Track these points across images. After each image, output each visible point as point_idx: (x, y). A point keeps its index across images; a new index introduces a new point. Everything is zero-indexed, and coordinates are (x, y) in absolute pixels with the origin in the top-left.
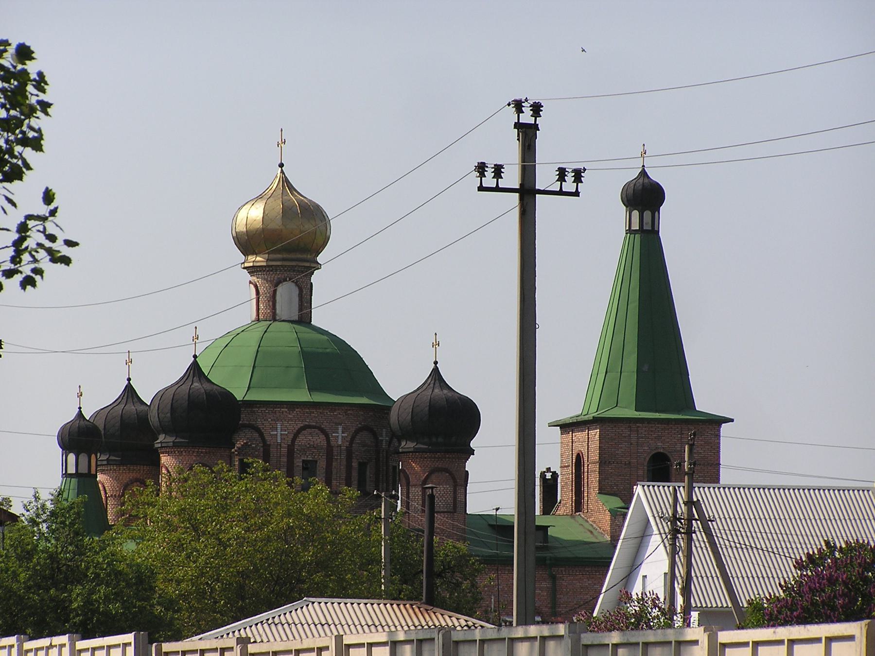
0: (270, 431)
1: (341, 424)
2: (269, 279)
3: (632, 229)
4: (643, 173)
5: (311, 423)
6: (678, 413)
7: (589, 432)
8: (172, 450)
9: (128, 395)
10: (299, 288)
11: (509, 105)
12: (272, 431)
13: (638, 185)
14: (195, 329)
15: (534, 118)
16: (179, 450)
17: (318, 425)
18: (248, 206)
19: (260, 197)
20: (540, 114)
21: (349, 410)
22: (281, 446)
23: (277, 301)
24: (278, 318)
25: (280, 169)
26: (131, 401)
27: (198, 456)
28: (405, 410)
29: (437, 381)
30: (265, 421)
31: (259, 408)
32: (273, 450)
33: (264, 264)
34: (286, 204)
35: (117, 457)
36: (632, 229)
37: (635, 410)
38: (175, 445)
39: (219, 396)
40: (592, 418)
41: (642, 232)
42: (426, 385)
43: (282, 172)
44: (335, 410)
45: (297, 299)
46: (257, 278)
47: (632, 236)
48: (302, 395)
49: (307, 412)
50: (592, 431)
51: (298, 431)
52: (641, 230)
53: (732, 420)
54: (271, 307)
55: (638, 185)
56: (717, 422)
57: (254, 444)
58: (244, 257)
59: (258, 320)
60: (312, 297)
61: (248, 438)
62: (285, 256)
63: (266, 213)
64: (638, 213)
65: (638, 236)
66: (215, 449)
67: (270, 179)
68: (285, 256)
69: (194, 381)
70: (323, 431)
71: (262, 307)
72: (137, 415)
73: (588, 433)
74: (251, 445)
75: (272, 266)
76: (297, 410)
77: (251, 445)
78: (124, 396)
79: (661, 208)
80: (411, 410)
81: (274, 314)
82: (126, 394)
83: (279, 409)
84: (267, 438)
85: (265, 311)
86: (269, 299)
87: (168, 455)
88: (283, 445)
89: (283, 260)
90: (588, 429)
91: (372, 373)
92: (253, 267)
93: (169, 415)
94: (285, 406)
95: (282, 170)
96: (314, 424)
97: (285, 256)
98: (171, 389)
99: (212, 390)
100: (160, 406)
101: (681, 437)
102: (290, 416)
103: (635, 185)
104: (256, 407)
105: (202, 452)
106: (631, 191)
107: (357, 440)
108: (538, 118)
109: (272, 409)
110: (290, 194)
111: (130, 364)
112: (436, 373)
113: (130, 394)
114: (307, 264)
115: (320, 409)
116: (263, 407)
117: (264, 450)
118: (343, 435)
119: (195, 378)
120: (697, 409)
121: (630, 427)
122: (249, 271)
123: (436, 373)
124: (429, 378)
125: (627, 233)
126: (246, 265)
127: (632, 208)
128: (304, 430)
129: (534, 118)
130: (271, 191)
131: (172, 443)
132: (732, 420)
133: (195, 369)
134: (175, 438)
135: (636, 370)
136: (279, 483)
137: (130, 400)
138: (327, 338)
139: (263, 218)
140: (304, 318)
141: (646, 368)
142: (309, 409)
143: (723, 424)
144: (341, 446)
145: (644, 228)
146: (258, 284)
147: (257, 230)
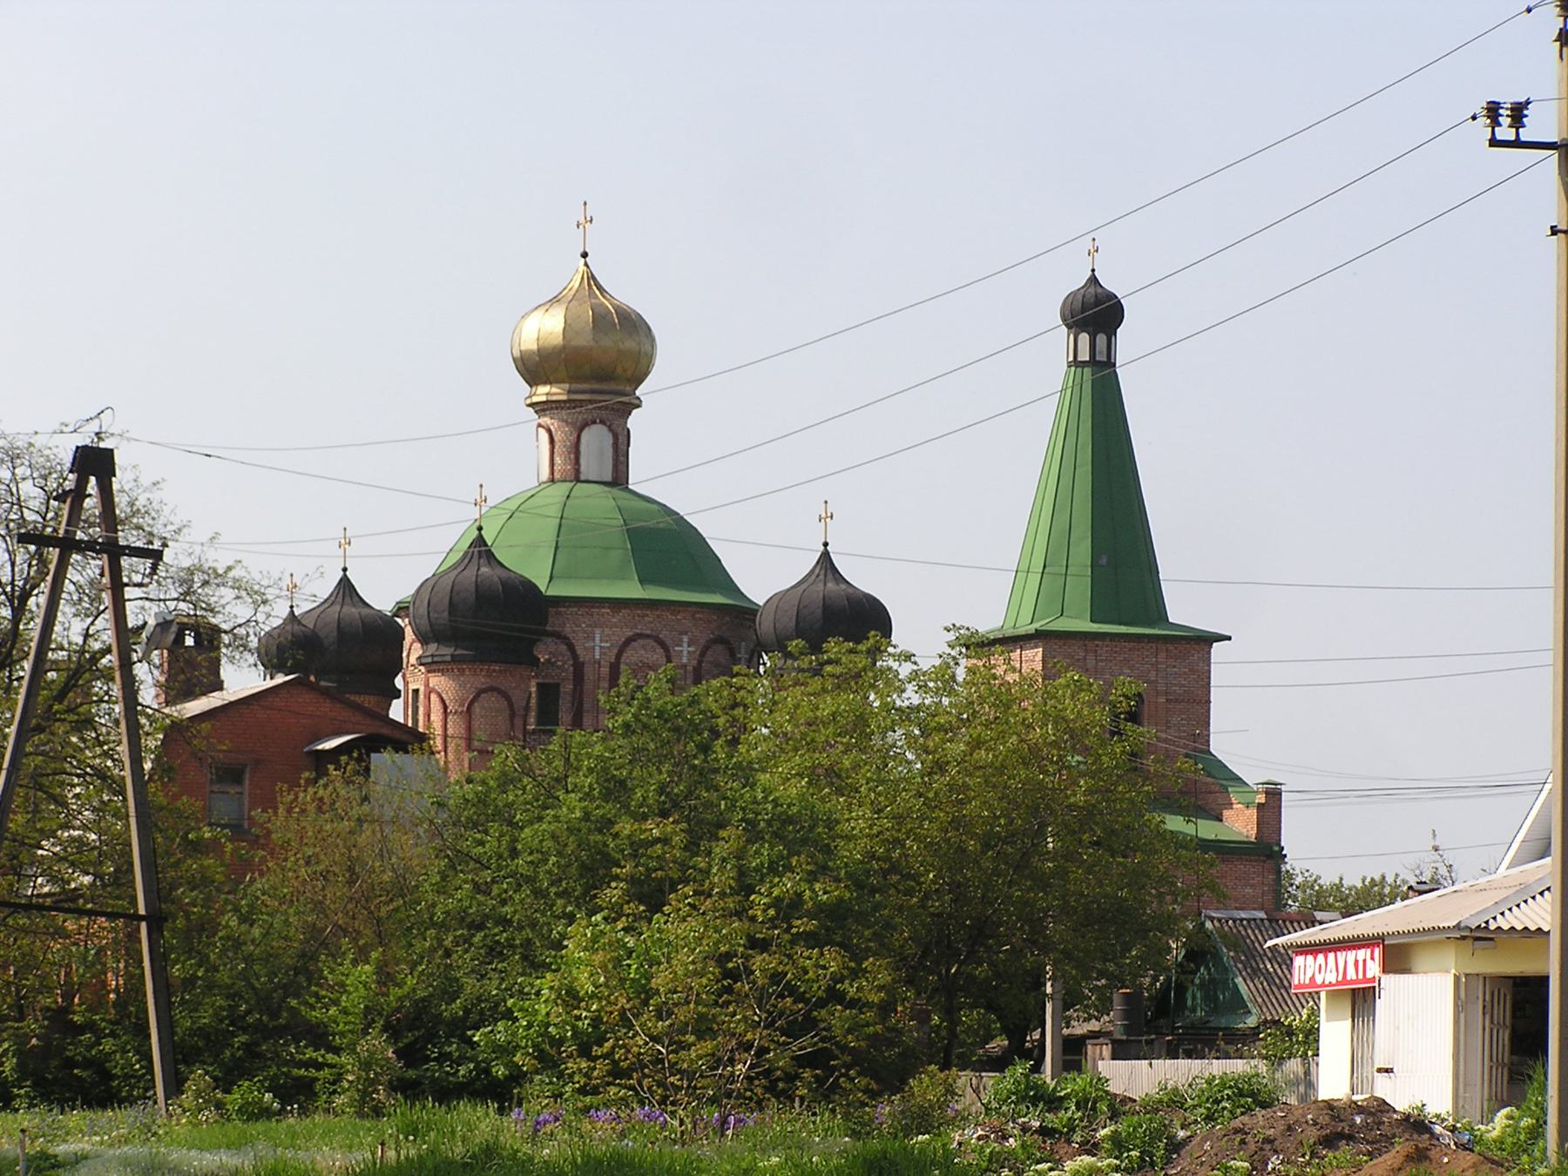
1: (686, 633)
3: (1079, 359)
4: (1093, 280)
6: (1150, 626)
9: (344, 593)
11: (1474, 118)
13: (1088, 296)
14: (479, 488)
15: (1514, 130)
17: (654, 634)
19: (555, 300)
20: (1523, 123)
25: (583, 260)
29: (829, 571)
33: (564, 397)
35: (467, 650)
36: (1079, 359)
37: (1091, 621)
38: (455, 659)
42: (814, 577)
43: (586, 264)
45: (611, 450)
47: (1079, 370)
48: (632, 589)
51: (625, 642)
52: (1093, 362)
53: (1229, 638)
56: (1205, 641)
59: (552, 480)
60: (630, 449)
61: (550, 653)
62: (596, 386)
63: (568, 322)
65: (1087, 371)
70: (662, 644)
74: (555, 662)
75: (574, 401)
77: (555, 662)
79: (1118, 330)
88: (602, 663)
89: (593, 392)
97: (596, 386)
98: (446, 577)
103: (1084, 296)
105: (494, 671)
106: (1078, 305)
107: (709, 657)
108: (1521, 130)
112: (825, 557)
113: (347, 592)
115: (657, 610)
117: (575, 669)
120: (1170, 620)
121: (1085, 645)
124: (815, 567)
125: (1069, 367)
126: (535, 399)
128: (635, 640)
129: (1514, 130)
130: (573, 292)
132: (1229, 638)
133: (480, 549)
135: (1089, 563)
137: (348, 599)
139: (564, 328)
140: (619, 478)
141: (1104, 561)
143: (1214, 644)
146: (552, 427)
147: (555, 347)
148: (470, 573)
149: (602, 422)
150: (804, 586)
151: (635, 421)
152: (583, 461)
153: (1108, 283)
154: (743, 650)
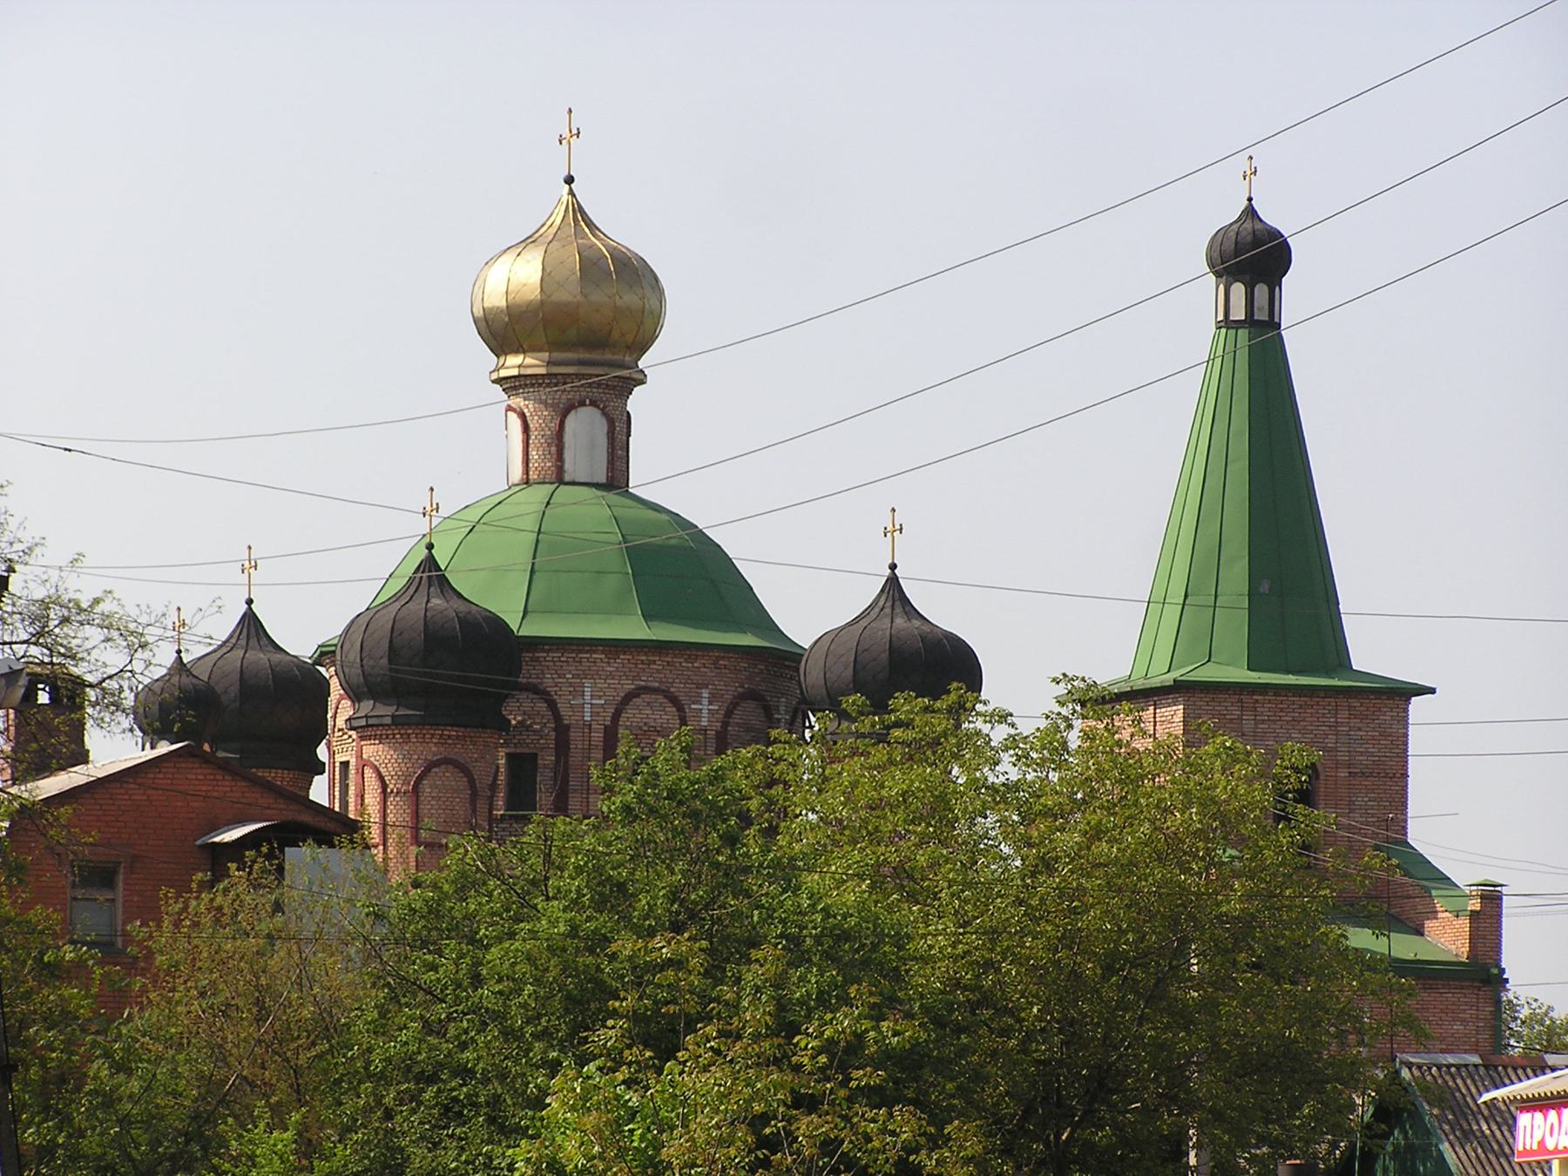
0: (571, 697)
2: (549, 401)
4: (1250, 212)
5: (649, 684)
7: (1158, 711)
8: (389, 732)
10: (608, 420)
12: (573, 700)
13: (1244, 233)
16: (402, 732)
18: (508, 259)
19: (529, 241)
21: (723, 658)
22: (590, 729)
23: (566, 445)
24: (567, 478)
26: (257, 644)
27: (442, 744)
28: (840, 657)
29: (897, 603)
30: (559, 678)
31: (548, 651)
32: (574, 735)
33: (542, 371)
34: (584, 254)
36: (1231, 318)
37: (1248, 669)
38: (397, 721)
39: (484, 624)
40: (1172, 683)
41: (1251, 326)
42: (877, 610)
43: (571, 193)
44: (696, 659)
46: (525, 399)
47: (1231, 332)
48: (634, 628)
49: (642, 662)
50: (1163, 710)
52: (1250, 321)
53: (1432, 691)
54: (555, 456)
55: (1226, 243)
56: (1401, 694)
57: (538, 724)
58: (496, 358)
59: (527, 482)
60: (631, 439)
64: (1243, 287)
65: (1243, 333)
66: (475, 730)
67: (550, 206)
68: (581, 356)
69: (431, 595)
70: (674, 701)
71: (536, 457)
72: (272, 670)
73: (1155, 713)
74: (531, 725)
75: (556, 375)
76: (622, 657)
77: (531, 725)
78: (240, 633)
79: (1284, 279)
80: (853, 659)
81: (560, 470)
82: (245, 630)
83: (588, 655)
84: (564, 711)
85: (542, 465)
86: (549, 441)
87: (380, 743)
90: (1155, 705)
91: (751, 589)
92: (519, 376)
93: (385, 661)
94: (601, 648)
95: (571, 189)
96: (657, 684)
99: (469, 613)
100: (364, 644)
101: (1337, 722)
102: (609, 669)
103: (1237, 234)
104: (543, 651)
105: (449, 736)
106: (1230, 245)
107: (736, 719)
109: (574, 655)
110: (590, 235)
111: (252, 570)
112: (893, 586)
114: (625, 373)
116: (557, 650)
118: (711, 707)
119: (432, 589)
120: (1354, 668)
122: (505, 386)
123: (893, 586)
126: (503, 373)
127: (1231, 279)
128: (637, 696)
131: (390, 718)
132: (1432, 691)
133: (430, 574)
134: (395, 707)
136: (809, 740)
137: (253, 642)
138: (668, 518)
140: (616, 479)
141: (1265, 587)
142: (646, 654)
143: (1413, 699)
144: (706, 730)
145: (1256, 318)
146: (526, 411)
148: (418, 606)
149: (593, 404)
150: (863, 623)
151: (637, 402)
152: (568, 456)
153: (1271, 216)
154: (782, 709)
